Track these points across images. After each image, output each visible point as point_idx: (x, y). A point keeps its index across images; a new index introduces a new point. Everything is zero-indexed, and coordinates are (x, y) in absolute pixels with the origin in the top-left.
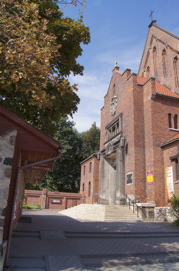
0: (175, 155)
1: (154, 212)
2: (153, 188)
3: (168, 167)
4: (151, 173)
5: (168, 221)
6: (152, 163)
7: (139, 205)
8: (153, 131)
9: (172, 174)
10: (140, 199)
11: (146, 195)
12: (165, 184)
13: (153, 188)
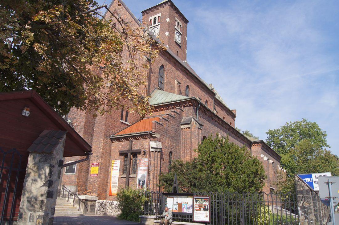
0: (124, 150)
1: (95, 205)
2: (97, 181)
3: (116, 160)
4: (97, 164)
5: (108, 215)
6: (100, 154)
7: (82, 197)
8: (106, 121)
9: (118, 168)
10: (81, 191)
11: (87, 187)
12: (109, 177)
13: (97, 181)
